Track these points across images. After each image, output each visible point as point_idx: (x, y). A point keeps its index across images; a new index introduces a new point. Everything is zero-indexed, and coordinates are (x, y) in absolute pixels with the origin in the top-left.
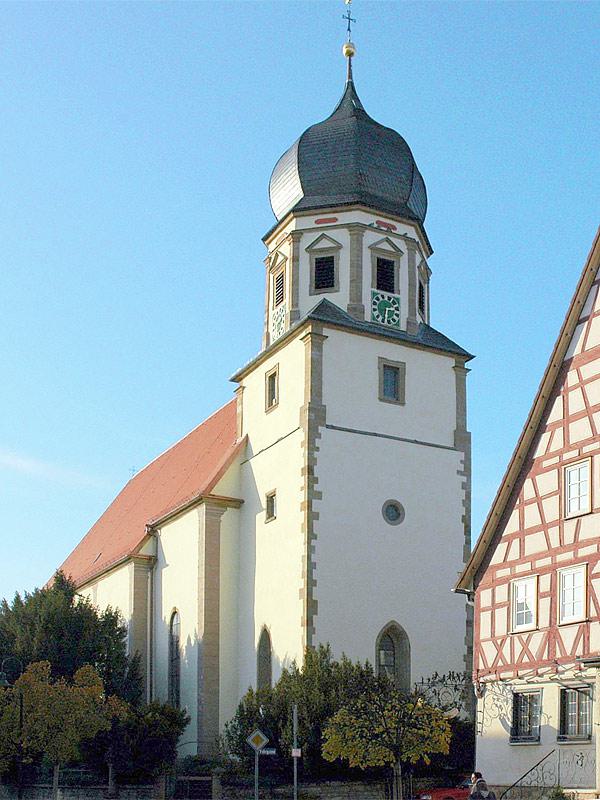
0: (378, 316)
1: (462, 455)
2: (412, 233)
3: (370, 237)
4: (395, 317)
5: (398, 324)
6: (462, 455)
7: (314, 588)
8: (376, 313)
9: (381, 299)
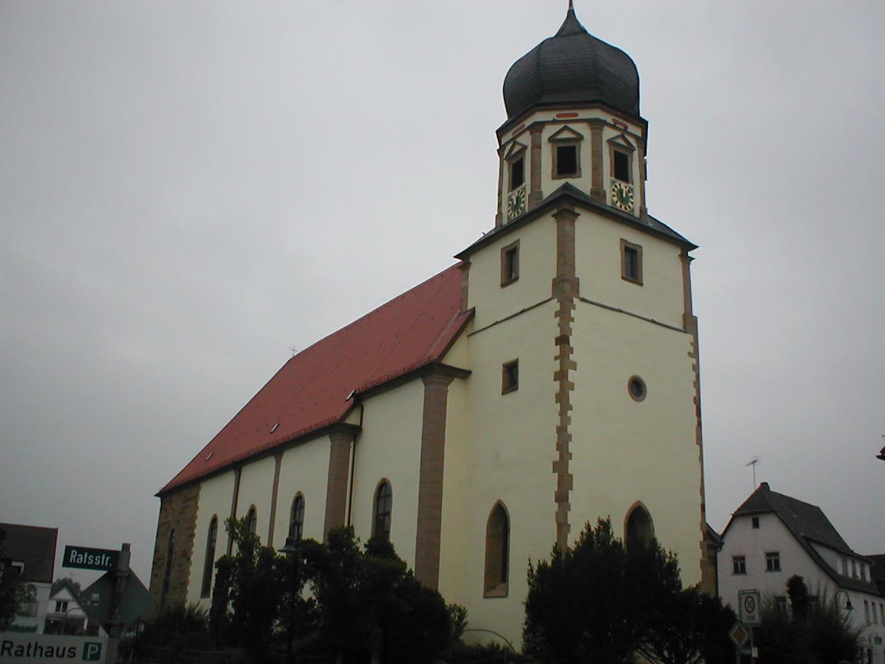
0: (617, 202)
1: (690, 337)
2: (638, 132)
3: (608, 133)
4: (630, 204)
5: (633, 210)
6: (173, 541)
7: (695, 395)
8: (615, 199)
9: (619, 187)
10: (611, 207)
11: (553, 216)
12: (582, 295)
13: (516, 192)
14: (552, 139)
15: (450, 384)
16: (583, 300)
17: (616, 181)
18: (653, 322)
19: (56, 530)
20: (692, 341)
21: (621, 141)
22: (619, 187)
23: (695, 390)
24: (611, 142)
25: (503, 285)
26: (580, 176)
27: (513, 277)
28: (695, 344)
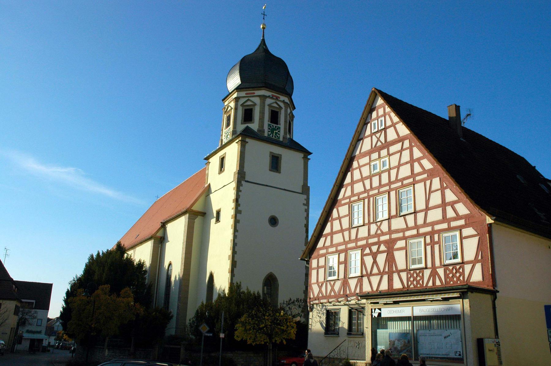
0: (270, 134)
1: (305, 197)
3: (268, 101)
8: (270, 133)
9: (272, 127)
10: (267, 137)
11: (236, 143)
12: (246, 179)
13: (227, 130)
14: (242, 105)
15: (196, 219)
16: (246, 181)
17: (271, 124)
18: (285, 190)
19: (51, 285)
20: (306, 198)
21: (275, 105)
22: (272, 127)
23: (306, 221)
24: (270, 105)
25: (219, 173)
26: (253, 123)
27: (222, 170)
28: (308, 200)
